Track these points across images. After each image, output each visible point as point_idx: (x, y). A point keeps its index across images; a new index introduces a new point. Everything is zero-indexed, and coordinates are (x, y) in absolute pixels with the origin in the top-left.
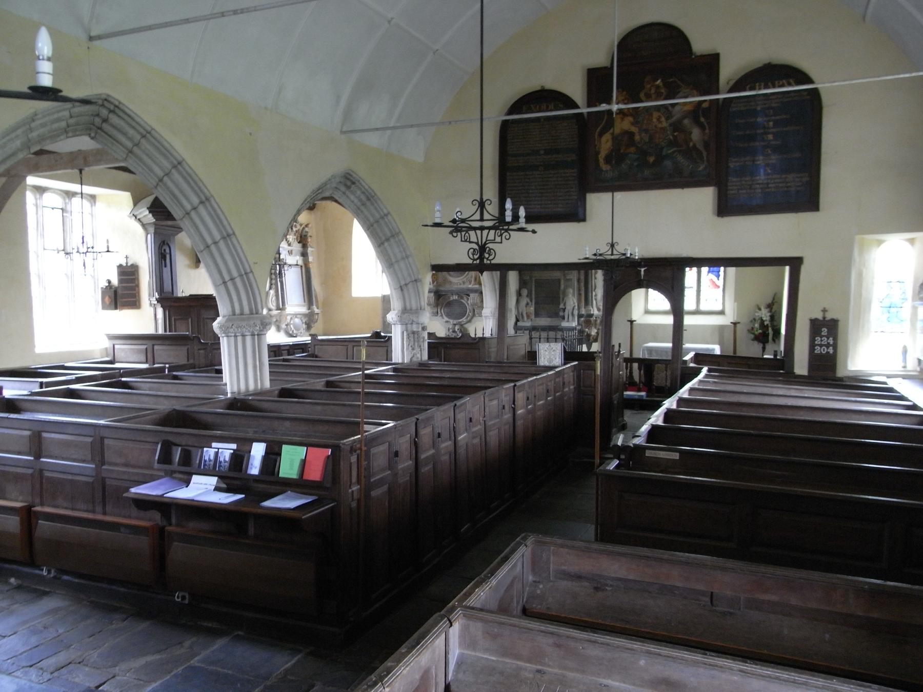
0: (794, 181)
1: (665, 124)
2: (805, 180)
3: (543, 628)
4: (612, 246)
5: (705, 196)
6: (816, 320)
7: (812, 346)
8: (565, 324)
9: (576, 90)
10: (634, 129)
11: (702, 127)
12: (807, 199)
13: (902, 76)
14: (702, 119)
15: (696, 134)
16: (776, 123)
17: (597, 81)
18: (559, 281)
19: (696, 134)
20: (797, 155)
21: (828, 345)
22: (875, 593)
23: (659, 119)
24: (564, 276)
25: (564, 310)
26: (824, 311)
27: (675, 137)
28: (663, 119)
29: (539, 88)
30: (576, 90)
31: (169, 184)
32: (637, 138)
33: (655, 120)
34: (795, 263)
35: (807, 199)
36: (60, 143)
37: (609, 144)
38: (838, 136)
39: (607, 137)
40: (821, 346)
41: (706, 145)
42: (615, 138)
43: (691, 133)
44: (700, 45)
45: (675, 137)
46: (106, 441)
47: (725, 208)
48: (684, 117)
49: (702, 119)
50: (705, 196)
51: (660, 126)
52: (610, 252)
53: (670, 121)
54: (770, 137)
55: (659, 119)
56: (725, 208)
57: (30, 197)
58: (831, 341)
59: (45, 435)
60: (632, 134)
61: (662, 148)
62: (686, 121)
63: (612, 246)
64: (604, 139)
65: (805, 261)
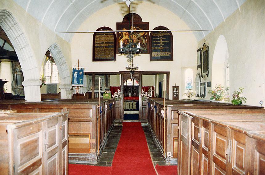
0: (168, 53)
1: (136, 38)
2: (170, 54)
3: (189, 135)
9: (114, 29)
10: (128, 39)
11: (145, 39)
12: (170, 58)
13: (219, 171)
14: (145, 38)
22: (85, 159)
23: (135, 37)
28: (136, 37)
30: (114, 29)
31: (17, 40)
32: (129, 41)
33: (134, 37)
34: (168, 73)
35: (170, 58)
41: (146, 44)
43: (143, 41)
46: (91, 110)
48: (141, 37)
49: (145, 38)
50: (148, 56)
51: (135, 38)
53: (138, 37)
54: (162, 43)
55: (135, 37)
57: (70, 75)
58: (177, 91)
59: (91, 110)
60: (128, 40)
61: (136, 44)
65: (170, 72)
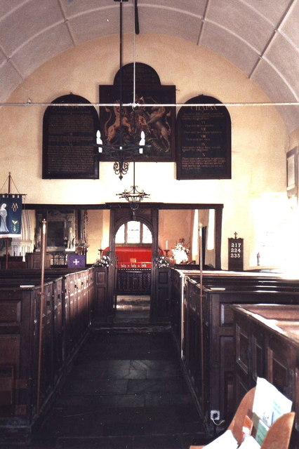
4: (134, 188)
5: (170, 168)
6: (232, 239)
7: (230, 253)
8: (67, 250)
10: (128, 125)
11: (167, 128)
12: (224, 171)
14: (167, 123)
15: (164, 131)
16: (207, 129)
17: (105, 93)
18: (63, 223)
19: (164, 131)
20: (219, 147)
21: (238, 248)
23: (142, 120)
24: (66, 218)
25: (67, 241)
26: (236, 234)
27: (152, 132)
29: (68, 93)
32: (130, 130)
34: (219, 208)
35: (224, 171)
36: (294, 178)
37: (113, 132)
38: (240, 139)
39: (112, 128)
40: (234, 253)
41: (169, 137)
42: (117, 130)
43: (161, 130)
44: (165, 80)
45: (152, 132)
47: (181, 174)
49: (167, 123)
50: (170, 168)
52: (133, 192)
54: (204, 136)
55: (142, 120)
56: (181, 174)
58: (239, 250)
60: (126, 128)
62: (158, 123)
63: (134, 188)
64: (110, 129)
